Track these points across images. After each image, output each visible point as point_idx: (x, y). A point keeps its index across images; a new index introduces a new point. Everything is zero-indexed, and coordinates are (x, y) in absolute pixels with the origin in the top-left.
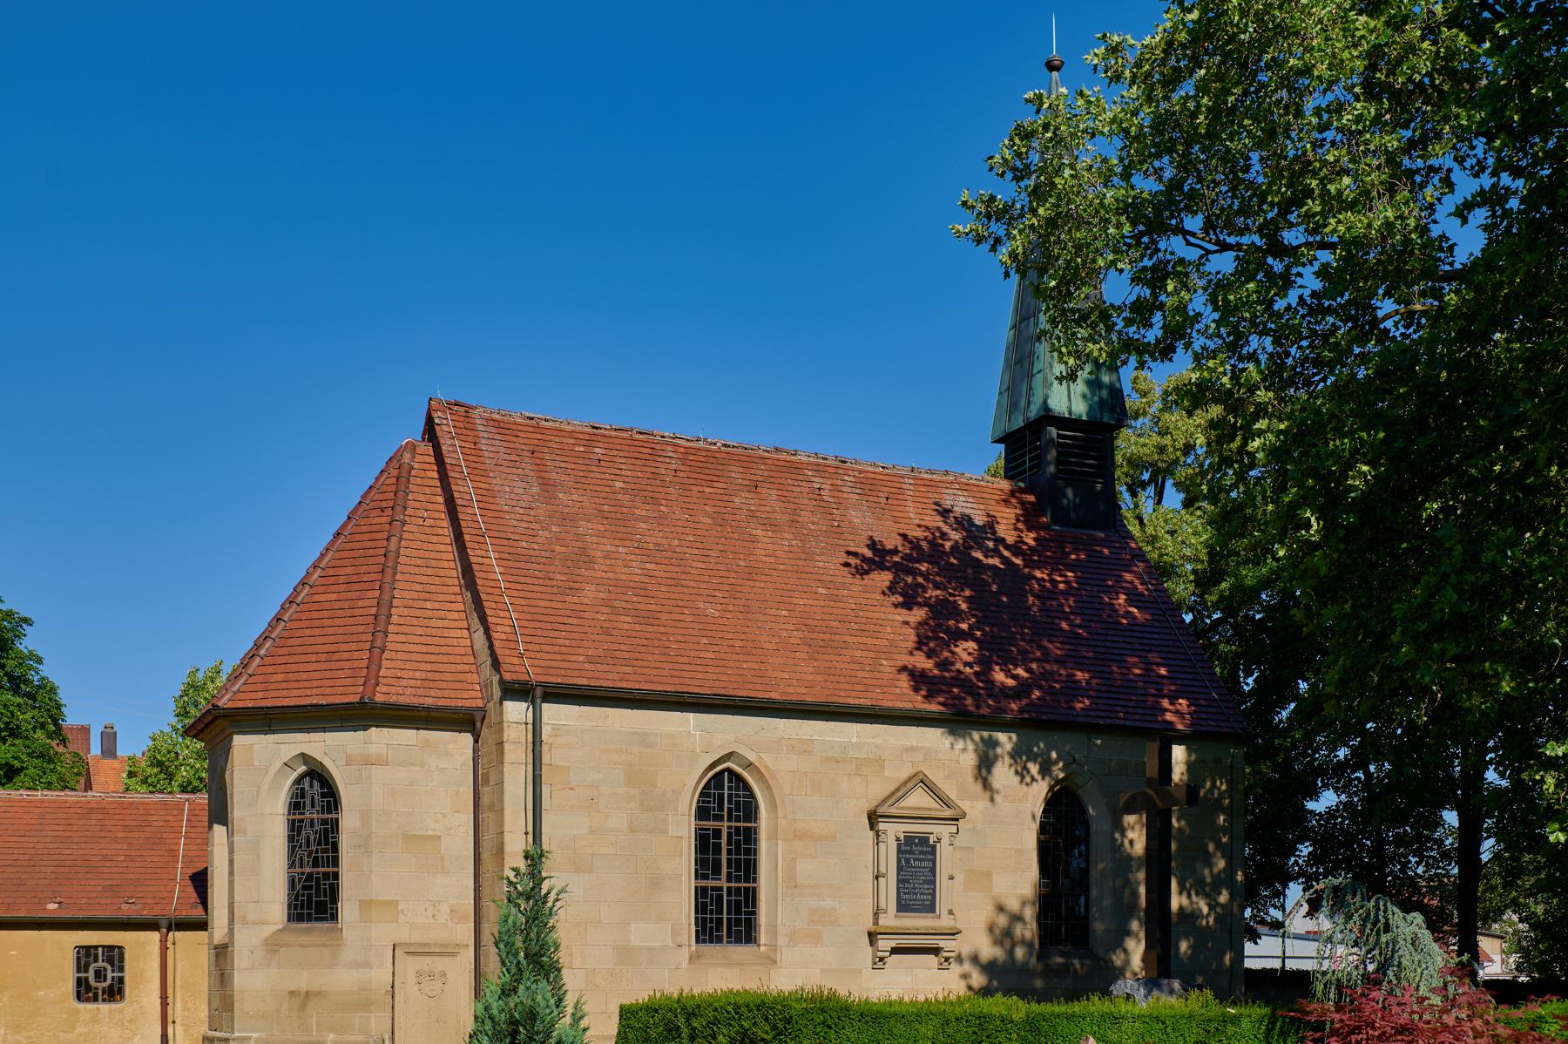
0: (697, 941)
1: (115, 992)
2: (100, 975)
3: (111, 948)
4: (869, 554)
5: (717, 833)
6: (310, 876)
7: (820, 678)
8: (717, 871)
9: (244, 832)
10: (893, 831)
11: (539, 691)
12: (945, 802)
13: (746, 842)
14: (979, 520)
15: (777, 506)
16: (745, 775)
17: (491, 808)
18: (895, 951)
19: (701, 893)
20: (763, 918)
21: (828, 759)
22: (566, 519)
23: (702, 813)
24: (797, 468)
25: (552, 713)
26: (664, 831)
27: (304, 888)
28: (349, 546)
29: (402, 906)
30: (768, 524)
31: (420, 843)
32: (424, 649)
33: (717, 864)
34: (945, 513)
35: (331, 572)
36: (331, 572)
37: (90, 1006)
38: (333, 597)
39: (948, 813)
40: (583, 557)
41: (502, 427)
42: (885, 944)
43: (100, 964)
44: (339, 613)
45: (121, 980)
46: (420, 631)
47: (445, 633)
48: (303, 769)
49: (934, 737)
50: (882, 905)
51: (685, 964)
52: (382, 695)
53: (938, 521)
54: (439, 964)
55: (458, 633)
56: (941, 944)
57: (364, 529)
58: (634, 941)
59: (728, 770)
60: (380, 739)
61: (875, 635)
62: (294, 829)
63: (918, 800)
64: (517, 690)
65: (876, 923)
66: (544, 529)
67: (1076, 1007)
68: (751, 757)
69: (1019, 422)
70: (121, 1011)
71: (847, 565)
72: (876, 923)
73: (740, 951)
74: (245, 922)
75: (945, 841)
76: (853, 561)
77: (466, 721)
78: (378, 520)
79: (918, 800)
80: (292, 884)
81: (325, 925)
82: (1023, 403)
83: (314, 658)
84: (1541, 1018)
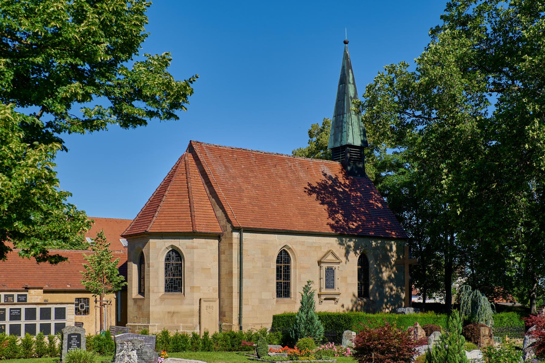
0: (277, 297)
1: (86, 312)
2: (82, 307)
3: (85, 299)
4: (309, 188)
5: (281, 267)
6: (172, 279)
7: (305, 224)
8: (281, 278)
9: (153, 267)
10: (325, 266)
11: (242, 230)
12: (337, 258)
13: (288, 269)
14: (334, 177)
15: (282, 171)
16: (288, 251)
17: (226, 261)
18: (325, 299)
19: (277, 283)
20: (292, 290)
21: (308, 246)
22: (234, 178)
23: (278, 262)
24: (283, 159)
25: (246, 235)
26: (270, 267)
27: (170, 282)
28: (175, 184)
29: (201, 288)
30: (281, 178)
31: (206, 270)
32: (204, 216)
33: (281, 275)
34: (325, 175)
35: (171, 192)
36: (171, 192)
37: (80, 316)
38: (174, 200)
39: (338, 261)
40: (240, 190)
41: (210, 149)
42: (323, 297)
43: (82, 303)
44: (177, 205)
45: (88, 308)
46: (202, 211)
47: (208, 211)
48: (171, 249)
49: (334, 241)
50: (322, 286)
51: (275, 303)
52: (199, 229)
53: (324, 178)
54: (212, 304)
55: (211, 211)
56: (336, 297)
57: (178, 179)
58: (263, 297)
59: (284, 250)
60: (197, 242)
61: (314, 211)
62: (167, 266)
63: (330, 257)
64: (235, 229)
65: (320, 291)
66: (230, 181)
67: (375, 316)
68: (290, 246)
69: (338, 145)
70: (88, 318)
71: (305, 192)
72: (320, 291)
73: (286, 299)
74: (153, 292)
75: (337, 269)
76: (306, 190)
77: (218, 237)
78: (182, 177)
79: (330, 257)
80: (166, 281)
81: (178, 293)
82: (339, 140)
83: (173, 218)
84: (502, 317)
